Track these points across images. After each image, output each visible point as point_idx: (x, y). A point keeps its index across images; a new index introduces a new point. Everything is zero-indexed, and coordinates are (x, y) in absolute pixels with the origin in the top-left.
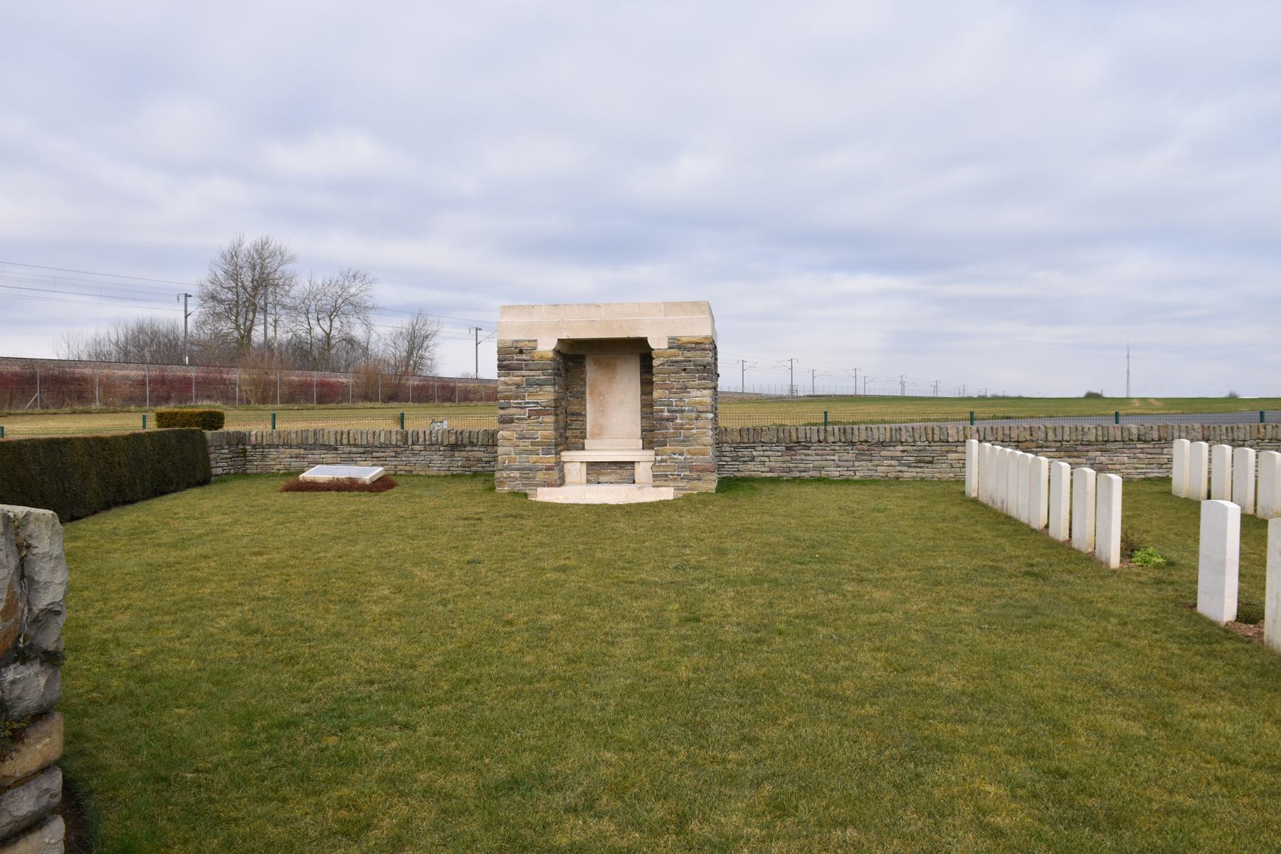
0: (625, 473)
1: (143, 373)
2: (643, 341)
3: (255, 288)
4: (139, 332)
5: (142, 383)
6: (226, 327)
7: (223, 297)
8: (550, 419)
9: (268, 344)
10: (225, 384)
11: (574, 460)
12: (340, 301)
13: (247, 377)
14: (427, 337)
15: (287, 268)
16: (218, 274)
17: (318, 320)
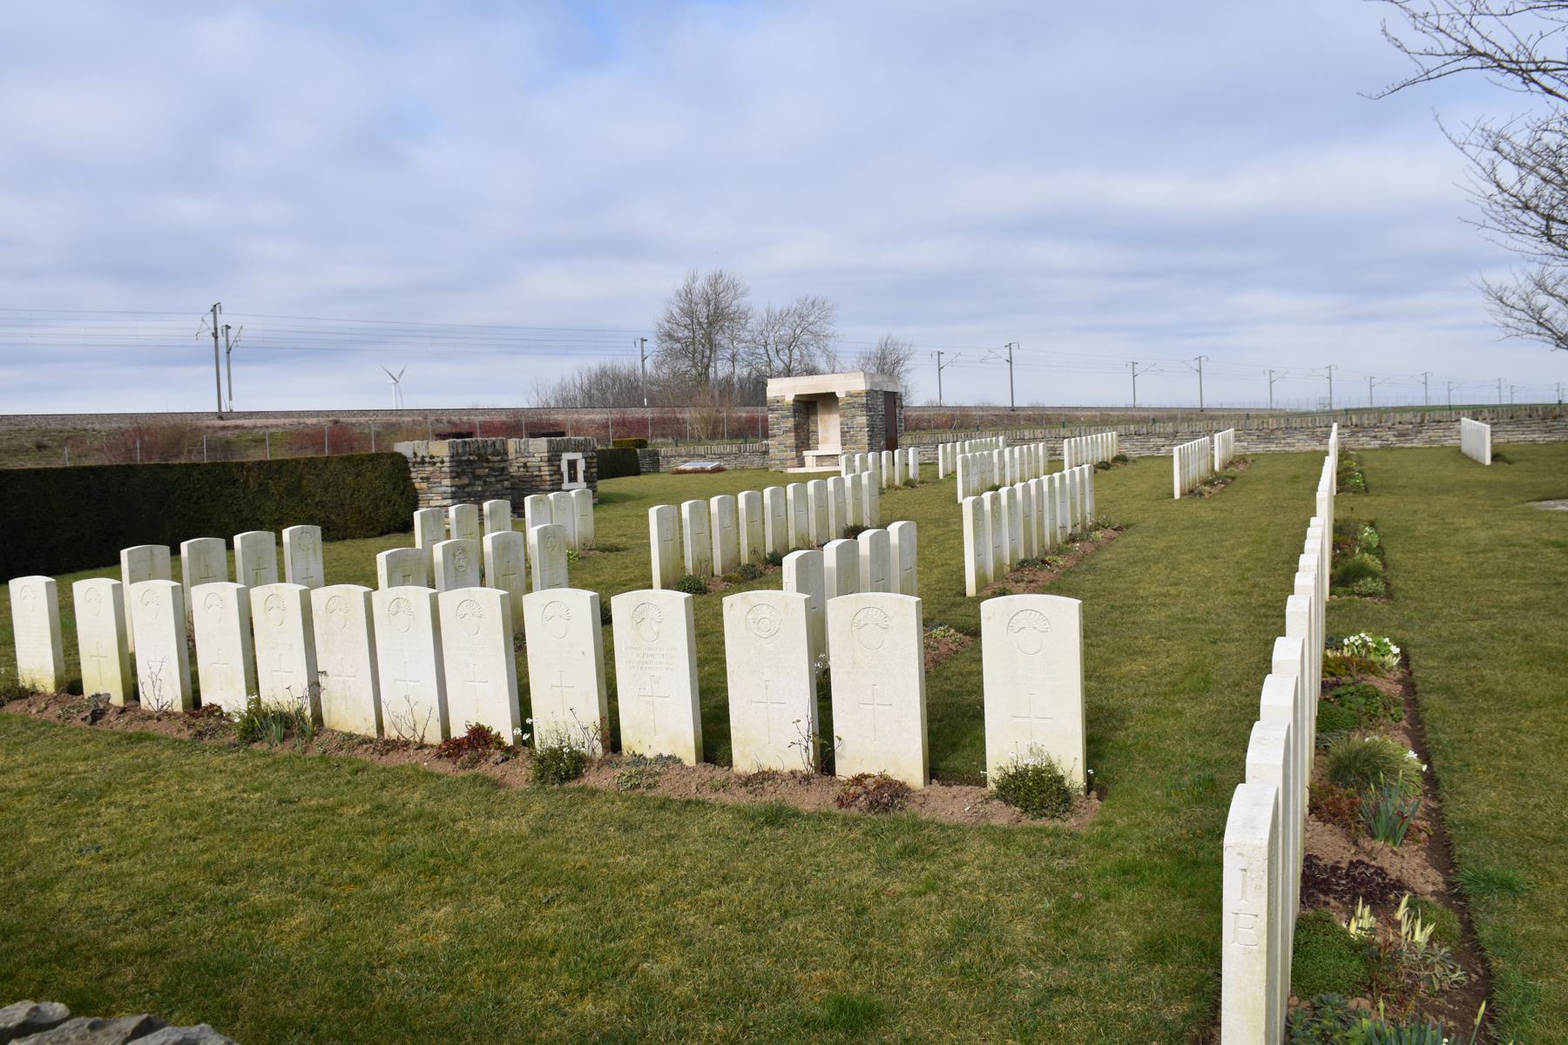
0: (834, 461)
1: (606, 416)
2: (833, 394)
3: (710, 324)
4: (602, 376)
5: (605, 426)
6: (684, 365)
7: (680, 335)
8: (793, 434)
9: (728, 381)
10: (679, 423)
11: (809, 455)
12: (798, 331)
13: (698, 416)
14: (898, 362)
15: (743, 302)
16: (674, 312)
17: (777, 352)
